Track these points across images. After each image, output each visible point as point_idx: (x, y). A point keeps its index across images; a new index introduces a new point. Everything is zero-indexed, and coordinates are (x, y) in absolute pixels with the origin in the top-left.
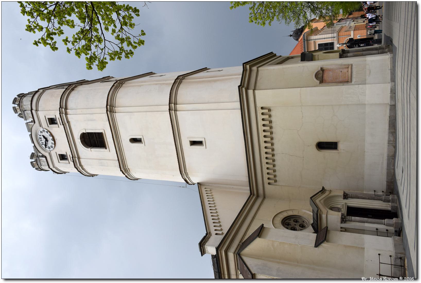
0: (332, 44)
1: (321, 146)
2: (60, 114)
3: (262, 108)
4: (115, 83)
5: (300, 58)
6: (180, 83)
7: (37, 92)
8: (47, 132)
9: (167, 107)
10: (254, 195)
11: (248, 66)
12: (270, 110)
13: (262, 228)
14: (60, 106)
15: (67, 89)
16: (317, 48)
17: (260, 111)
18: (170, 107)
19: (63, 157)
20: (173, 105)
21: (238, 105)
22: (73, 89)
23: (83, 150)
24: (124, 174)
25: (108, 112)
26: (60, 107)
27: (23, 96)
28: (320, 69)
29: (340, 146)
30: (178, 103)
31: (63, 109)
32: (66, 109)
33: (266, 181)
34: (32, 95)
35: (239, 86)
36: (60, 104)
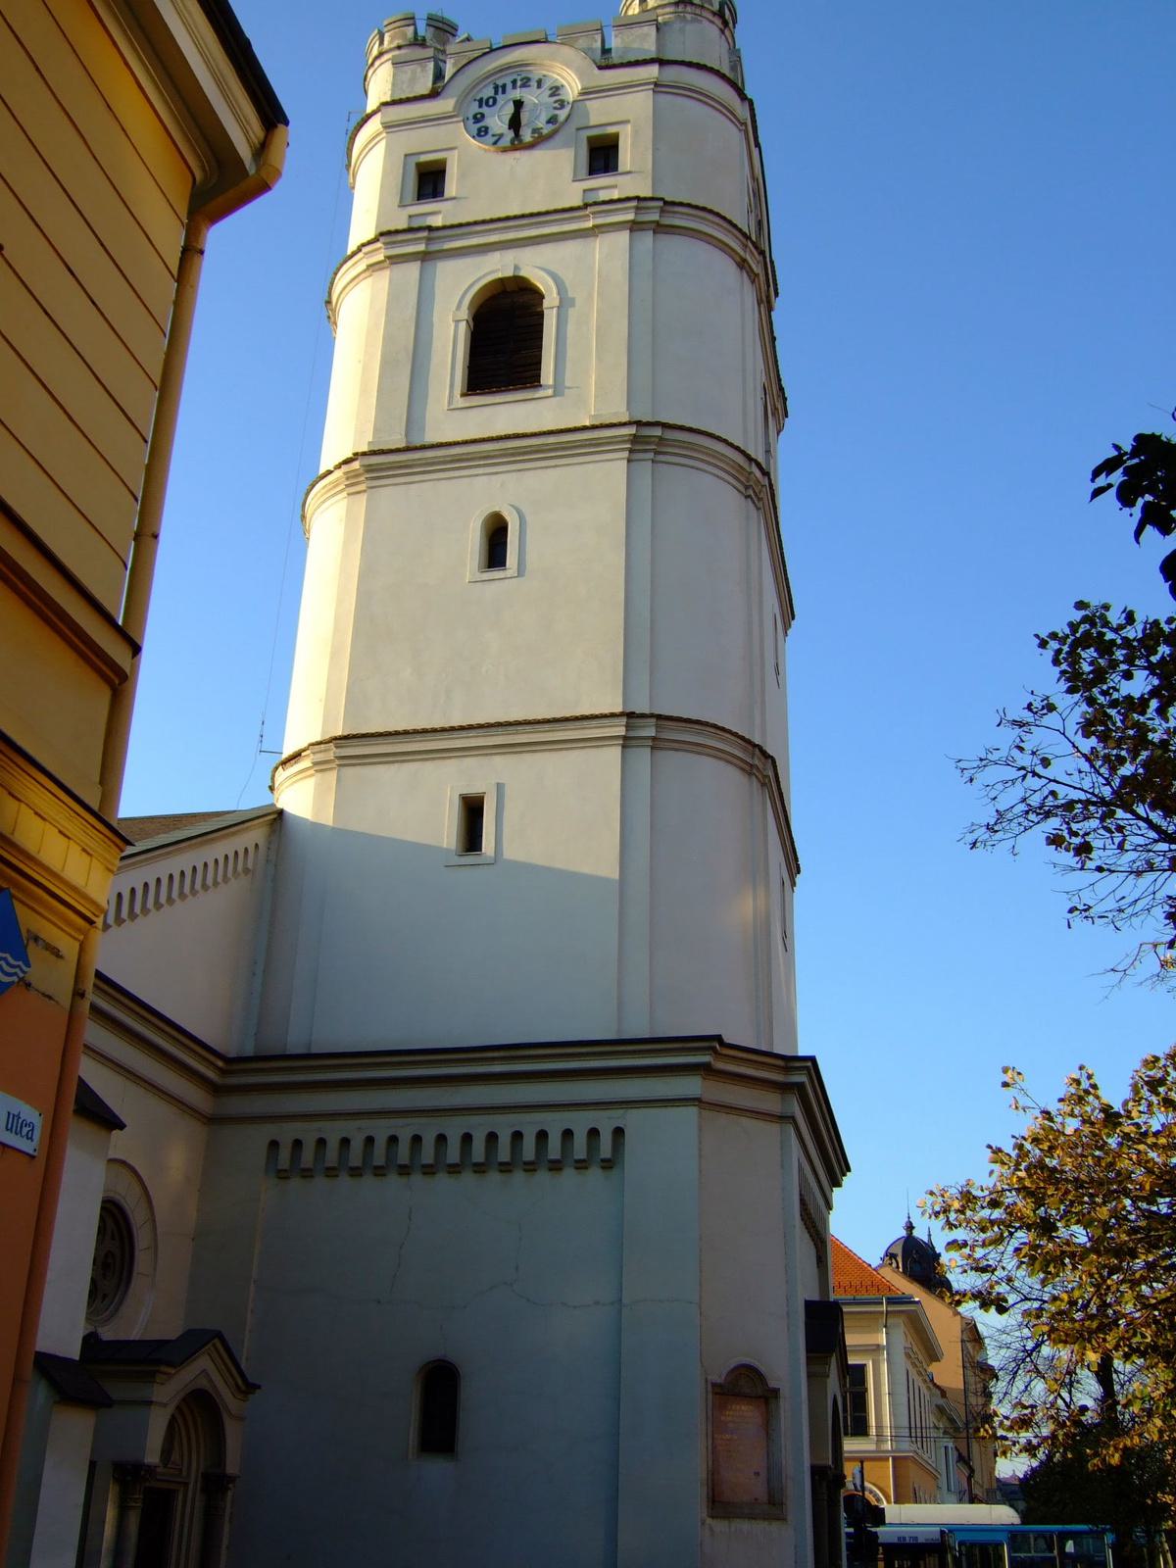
0: (860, 1429)
1: (440, 1384)
2: (638, 198)
3: (619, 1132)
4: (758, 465)
5: (815, 1297)
6: (749, 770)
7: (740, 92)
8: (552, 120)
9: (642, 707)
10: (223, 1072)
11: (802, 1078)
12: (608, 1165)
13: (109, 1121)
14: (673, 204)
15: (747, 237)
16: (852, 1360)
17: (605, 1122)
18: (643, 716)
19: (429, 180)
20: (651, 732)
21: (638, 1028)
22: (742, 264)
23: (459, 284)
24: (338, 467)
25: (632, 430)
26: (666, 203)
27: (725, 23)
28: (772, 1384)
29: (436, 1468)
30: (660, 754)
31: (655, 217)
32: (659, 228)
33: (287, 1133)
34: (726, 70)
35: (718, 1038)
36: (681, 204)
